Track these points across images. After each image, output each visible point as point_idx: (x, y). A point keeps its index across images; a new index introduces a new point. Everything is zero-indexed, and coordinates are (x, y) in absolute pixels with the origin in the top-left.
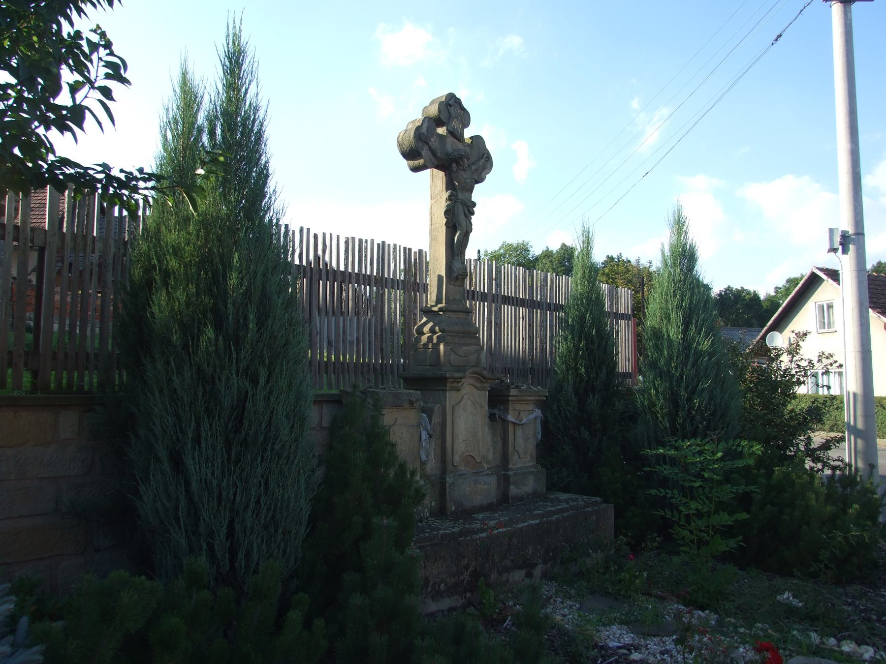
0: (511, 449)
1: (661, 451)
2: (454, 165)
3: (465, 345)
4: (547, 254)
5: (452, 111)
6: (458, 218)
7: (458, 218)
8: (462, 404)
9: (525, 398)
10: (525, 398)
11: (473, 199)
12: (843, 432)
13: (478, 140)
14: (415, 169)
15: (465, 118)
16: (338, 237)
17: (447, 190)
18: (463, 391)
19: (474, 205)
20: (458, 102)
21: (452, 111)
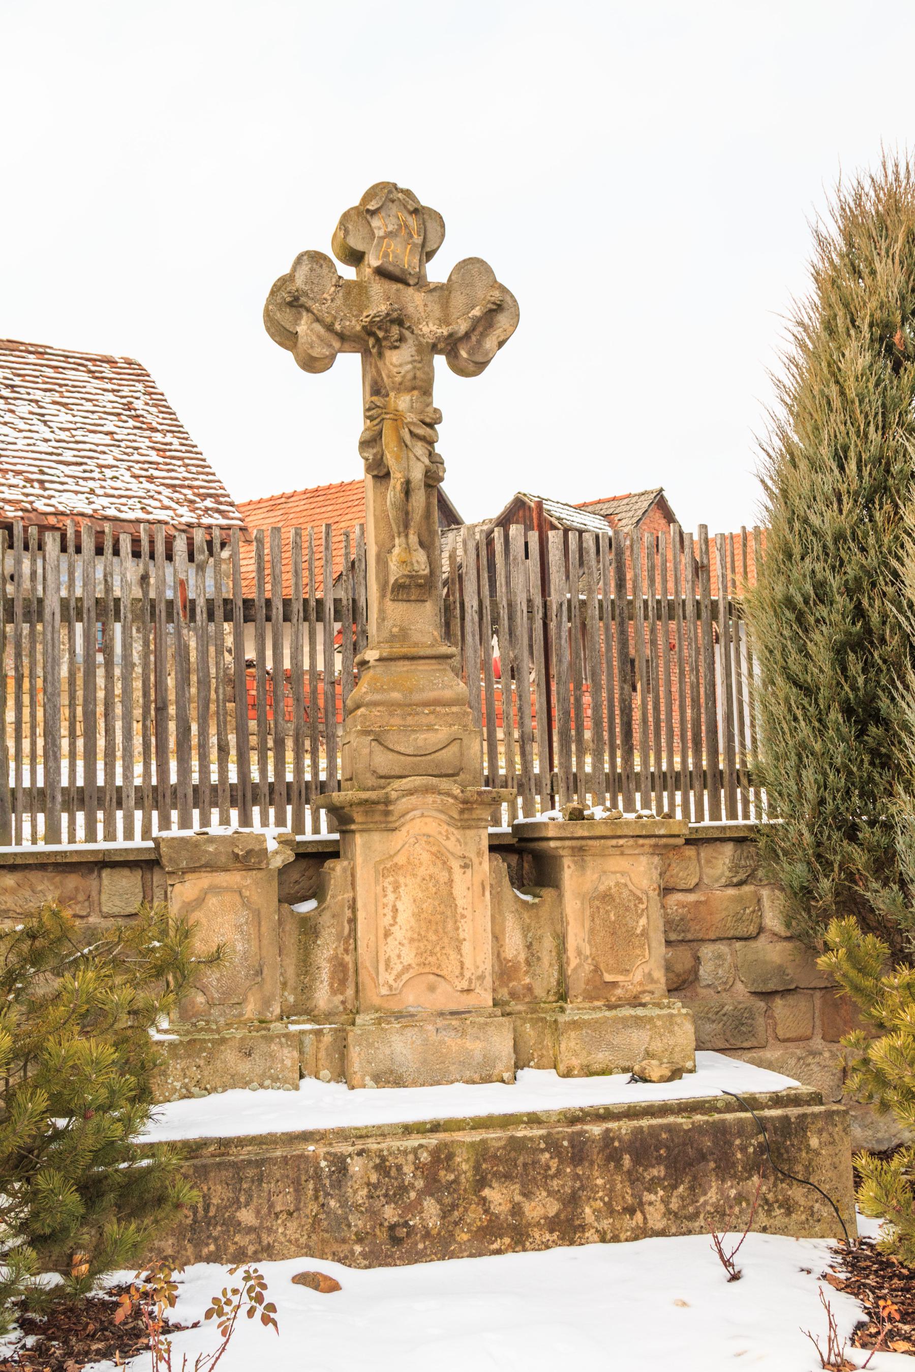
5: (393, 217)
11: (436, 405)
13: (473, 269)
21: (393, 217)
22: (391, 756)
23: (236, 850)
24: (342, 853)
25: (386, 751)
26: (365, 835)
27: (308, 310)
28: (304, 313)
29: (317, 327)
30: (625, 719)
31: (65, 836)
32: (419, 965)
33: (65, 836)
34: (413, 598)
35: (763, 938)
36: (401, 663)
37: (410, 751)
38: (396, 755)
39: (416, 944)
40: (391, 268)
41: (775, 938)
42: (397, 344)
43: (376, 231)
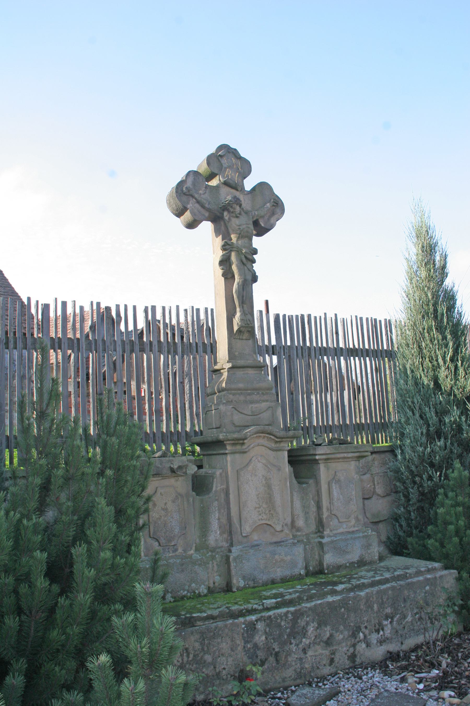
0: (325, 514)
1: (218, 532)
2: (225, 213)
3: (252, 402)
4: (253, 267)
5: (227, 161)
6: (238, 268)
7: (238, 268)
8: (250, 468)
9: (338, 456)
10: (338, 456)
11: (254, 246)
12: (390, 442)
13: (263, 188)
14: (191, 225)
15: (245, 167)
16: (135, 307)
17: (217, 236)
18: (252, 454)
19: (255, 252)
20: (234, 153)
21: (227, 161)
22: (242, 416)
23: (172, 466)
24: (204, 466)
25: (239, 414)
26: (232, 455)
27: (193, 197)
28: (191, 198)
29: (197, 205)
30: (175, 413)
31: (380, 442)
32: (259, 520)
33: (380, 442)
34: (244, 338)
35: (375, 498)
36: (250, 369)
37: (250, 413)
38: (244, 416)
39: (258, 510)
40: (231, 182)
41: (379, 497)
42: (238, 215)
43: (224, 165)
